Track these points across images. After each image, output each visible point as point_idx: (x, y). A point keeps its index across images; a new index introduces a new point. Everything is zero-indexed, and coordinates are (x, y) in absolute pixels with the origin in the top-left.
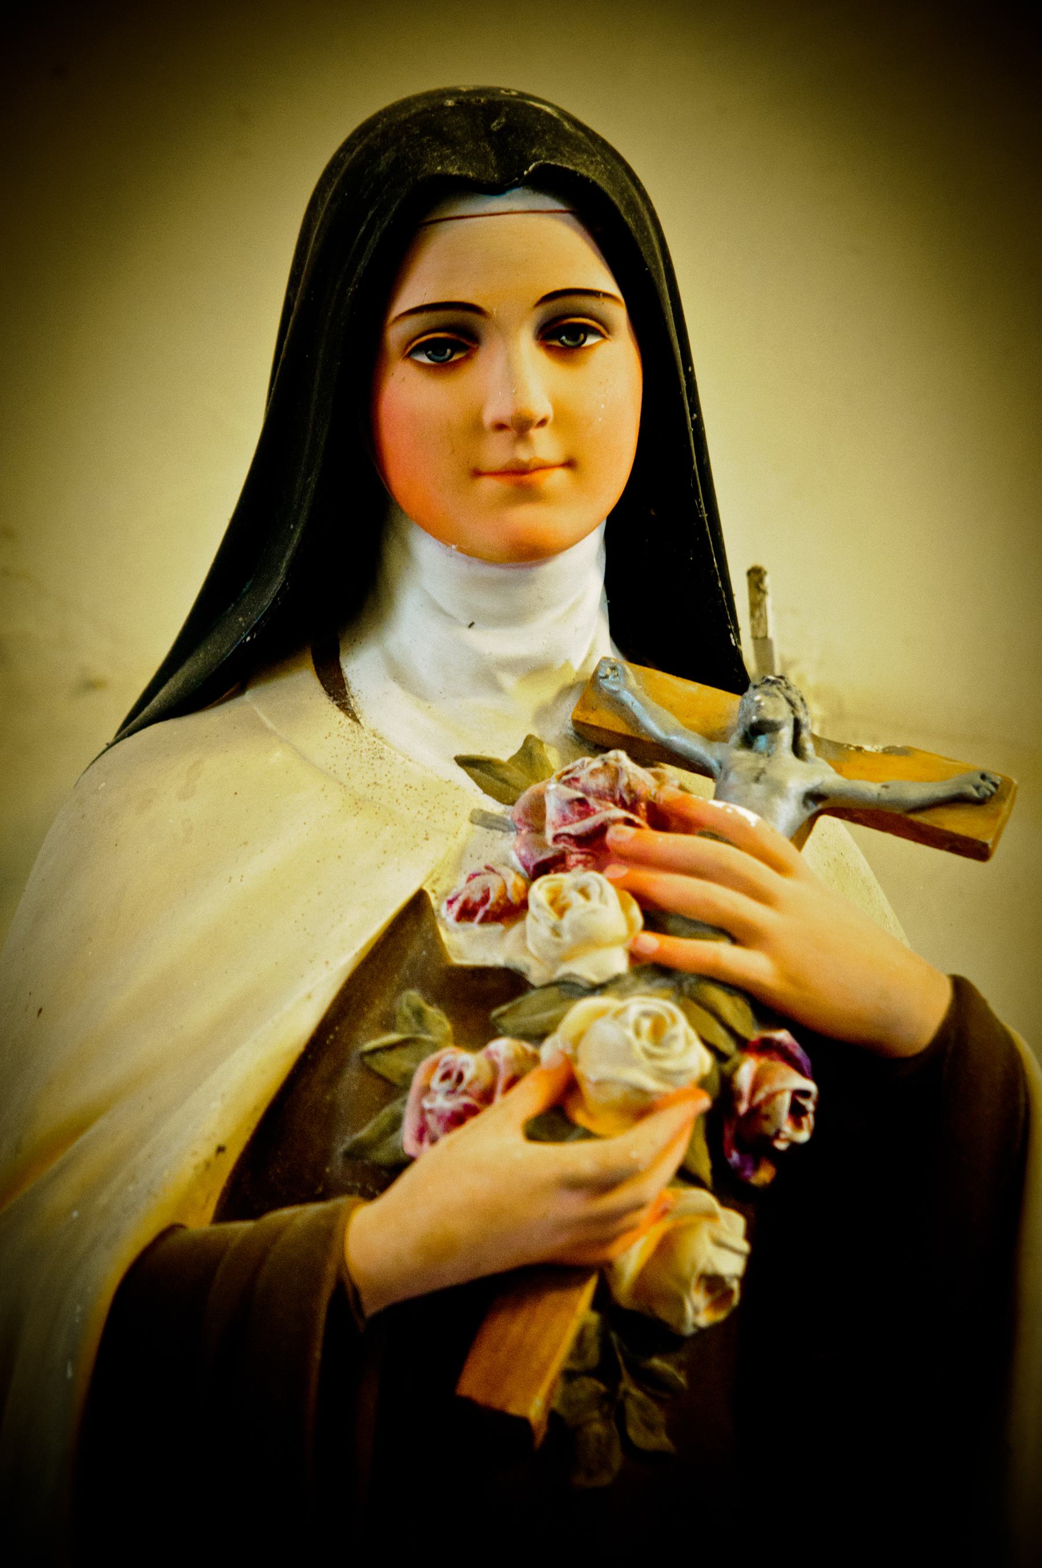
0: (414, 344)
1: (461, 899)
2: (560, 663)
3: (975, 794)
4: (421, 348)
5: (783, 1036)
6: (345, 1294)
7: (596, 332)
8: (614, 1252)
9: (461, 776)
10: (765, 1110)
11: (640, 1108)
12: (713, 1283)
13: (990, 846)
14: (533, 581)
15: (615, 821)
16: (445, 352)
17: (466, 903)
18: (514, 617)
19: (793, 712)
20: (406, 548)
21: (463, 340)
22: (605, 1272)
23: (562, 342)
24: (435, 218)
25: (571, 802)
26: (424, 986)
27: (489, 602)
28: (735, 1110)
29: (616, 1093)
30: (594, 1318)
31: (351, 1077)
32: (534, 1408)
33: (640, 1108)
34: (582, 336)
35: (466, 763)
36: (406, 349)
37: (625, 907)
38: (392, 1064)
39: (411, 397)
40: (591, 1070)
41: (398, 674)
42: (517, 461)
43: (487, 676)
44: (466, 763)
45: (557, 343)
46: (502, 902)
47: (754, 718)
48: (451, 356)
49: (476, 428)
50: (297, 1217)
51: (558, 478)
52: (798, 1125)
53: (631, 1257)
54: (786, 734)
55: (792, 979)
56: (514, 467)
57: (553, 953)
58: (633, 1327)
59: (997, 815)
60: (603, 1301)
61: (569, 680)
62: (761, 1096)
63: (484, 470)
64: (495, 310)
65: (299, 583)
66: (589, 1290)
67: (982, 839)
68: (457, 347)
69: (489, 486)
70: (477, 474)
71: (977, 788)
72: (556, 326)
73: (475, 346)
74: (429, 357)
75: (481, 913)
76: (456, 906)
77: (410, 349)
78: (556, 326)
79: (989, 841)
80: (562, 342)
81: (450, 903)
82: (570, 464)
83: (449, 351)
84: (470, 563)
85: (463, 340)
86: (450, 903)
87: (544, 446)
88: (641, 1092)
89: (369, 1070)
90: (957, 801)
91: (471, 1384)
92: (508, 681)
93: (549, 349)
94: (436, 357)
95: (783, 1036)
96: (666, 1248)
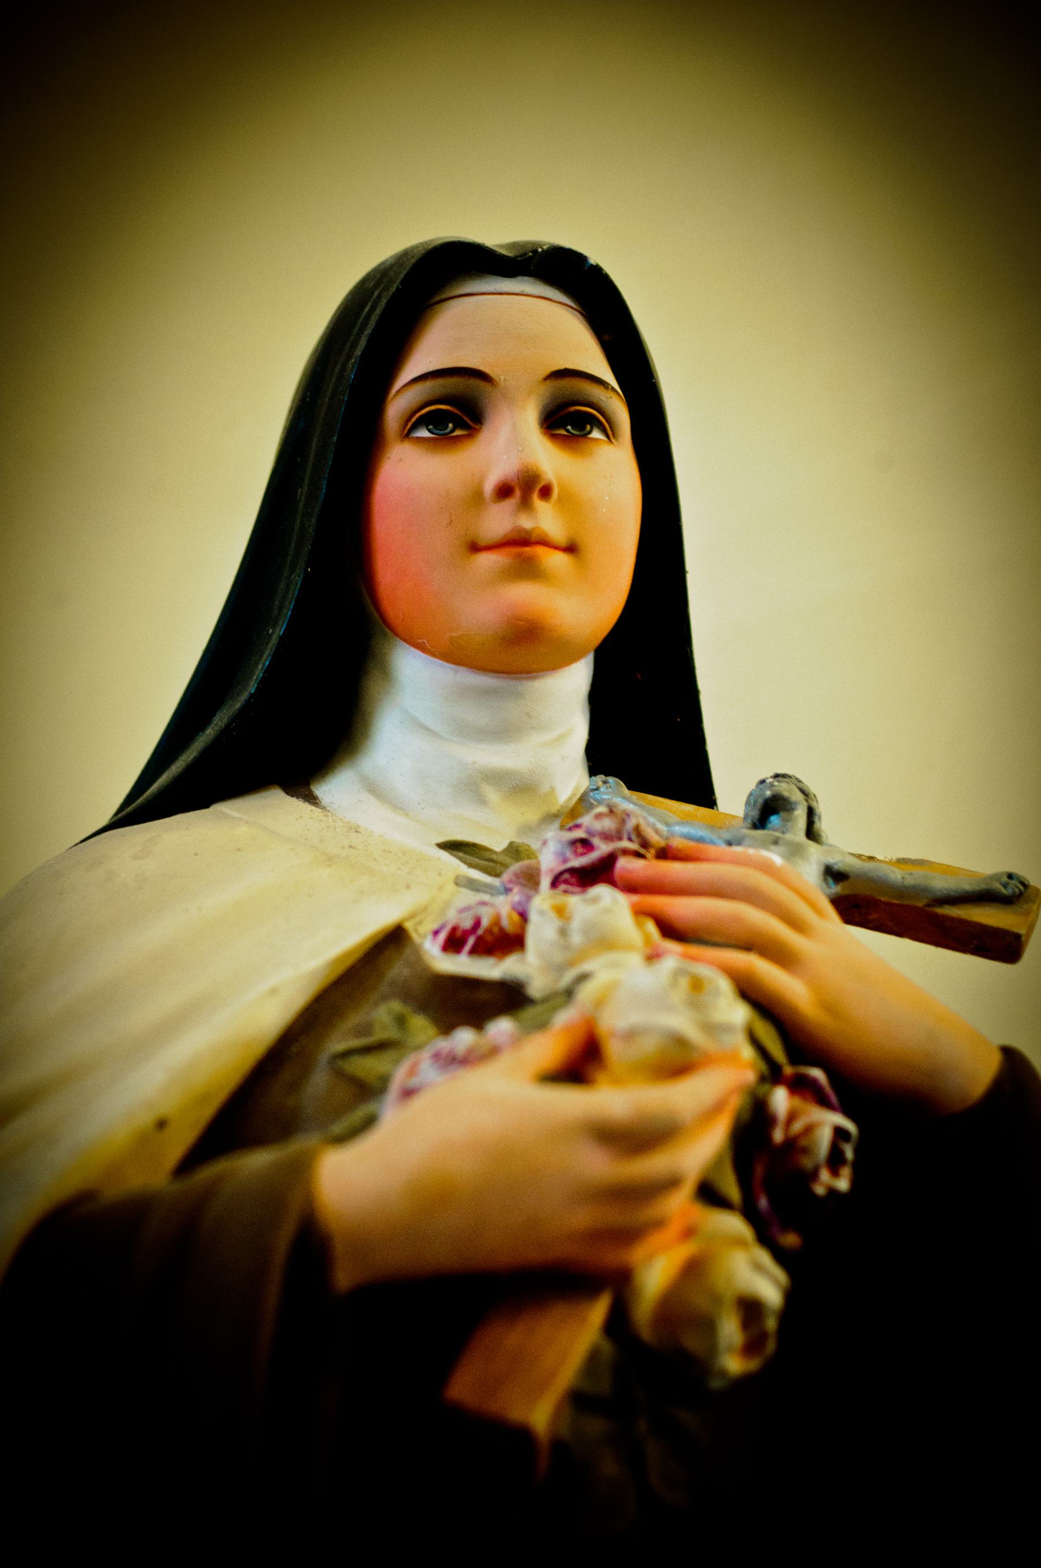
0: (414, 419)
1: (448, 928)
2: (545, 788)
3: (1004, 891)
4: (424, 421)
5: (817, 1073)
6: (312, 1241)
7: (604, 431)
8: (637, 1254)
9: (445, 856)
10: (803, 1142)
11: (677, 1062)
12: (750, 1309)
13: (1023, 939)
14: (519, 695)
15: (625, 852)
16: (447, 427)
17: (454, 929)
18: (503, 732)
19: (806, 800)
20: (386, 673)
21: (466, 419)
22: (620, 1283)
23: (568, 431)
24: (444, 296)
25: (574, 843)
26: (406, 995)
27: (478, 715)
28: (769, 1137)
29: (649, 1046)
30: (607, 1347)
31: (319, 1080)
32: (541, 1415)
33: (677, 1062)
34: (588, 427)
35: (453, 847)
36: (409, 419)
37: (639, 925)
38: (366, 1066)
39: (410, 475)
40: (613, 1022)
41: (375, 789)
42: (520, 530)
43: (474, 786)
44: (453, 847)
45: (564, 433)
46: (496, 930)
47: (768, 793)
48: (452, 431)
49: (476, 498)
50: (256, 1162)
51: (556, 561)
52: (835, 1173)
53: (656, 1272)
54: (800, 815)
55: (830, 1008)
56: (516, 536)
57: (559, 957)
58: (651, 1365)
59: (1027, 913)
60: (618, 1323)
61: (554, 810)
62: (797, 1127)
63: (482, 543)
64: (502, 378)
65: (277, 702)
66: (598, 1311)
67: (1015, 930)
68: (459, 424)
69: (487, 560)
70: (475, 548)
71: (1005, 886)
72: (564, 412)
73: (477, 427)
74: (430, 431)
75: (471, 941)
76: (442, 936)
77: (410, 425)
78: (564, 412)
79: (1022, 931)
80: (568, 431)
81: (436, 933)
82: (571, 549)
83: (451, 425)
84: (456, 671)
85: (466, 419)
86: (436, 933)
87: (546, 519)
88: (680, 1042)
89: (340, 1075)
90: (985, 897)
91: (463, 1387)
92: (492, 794)
93: (554, 437)
94: (435, 431)
95: (817, 1073)
96: (694, 1270)
